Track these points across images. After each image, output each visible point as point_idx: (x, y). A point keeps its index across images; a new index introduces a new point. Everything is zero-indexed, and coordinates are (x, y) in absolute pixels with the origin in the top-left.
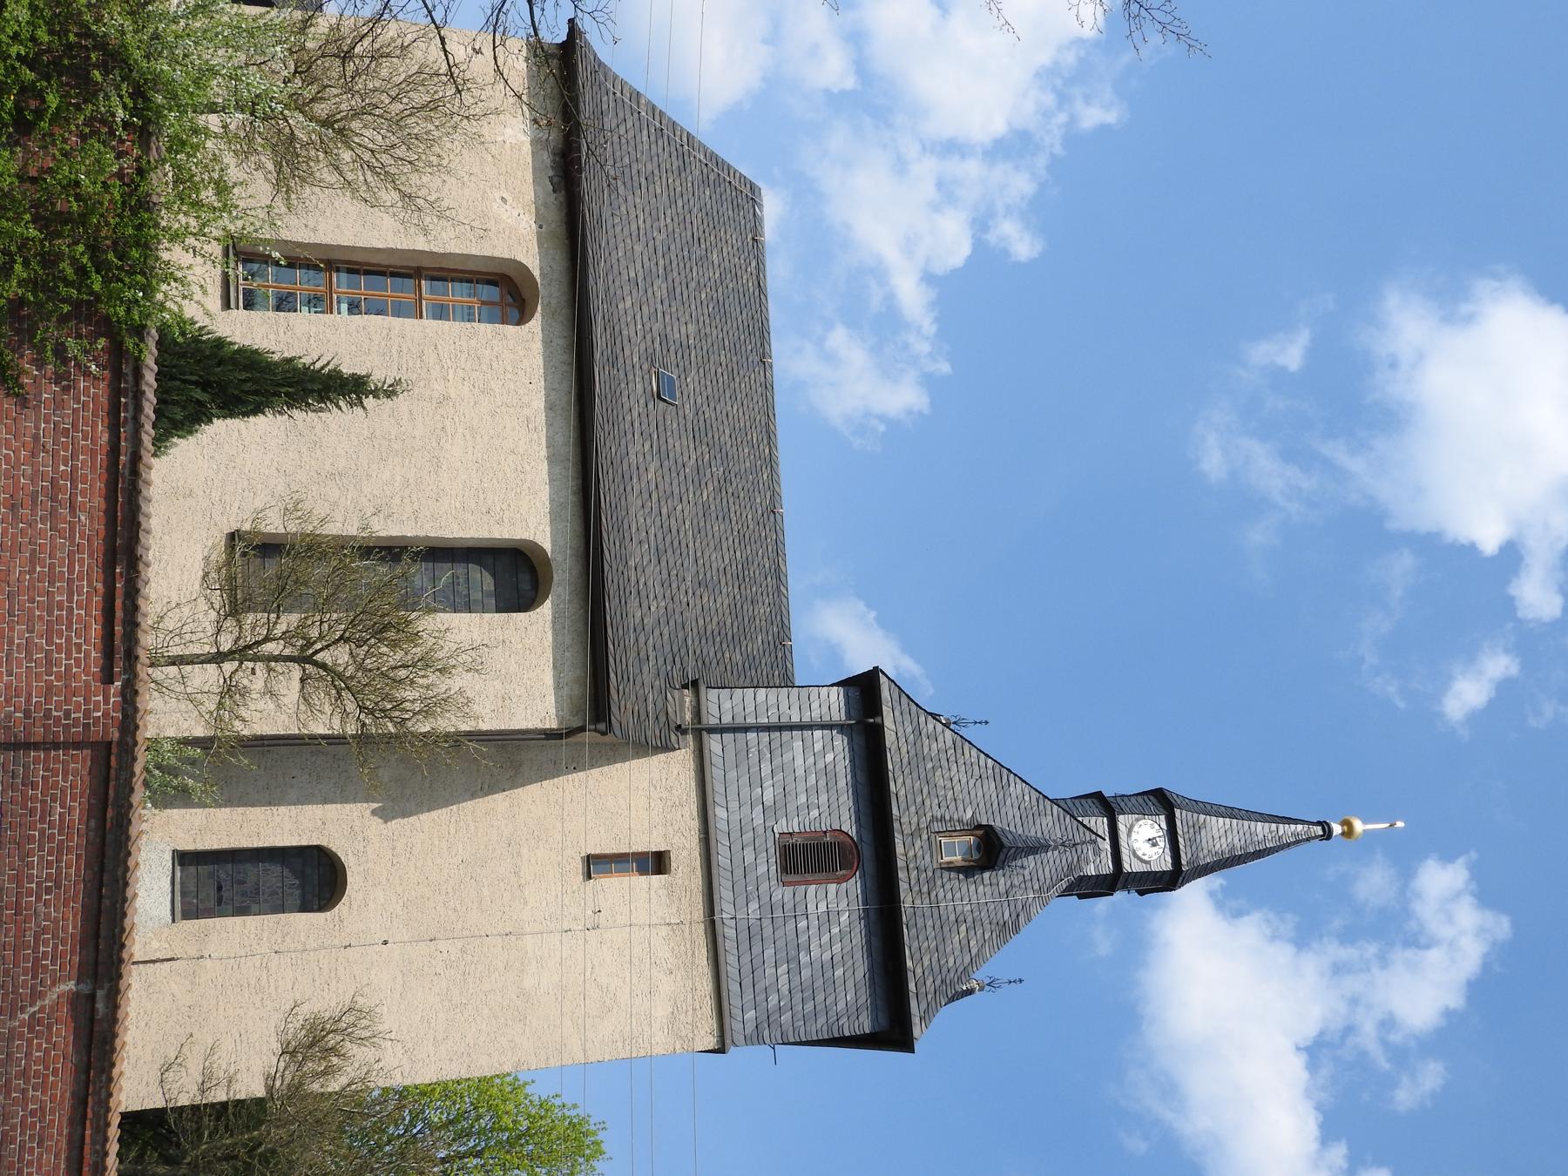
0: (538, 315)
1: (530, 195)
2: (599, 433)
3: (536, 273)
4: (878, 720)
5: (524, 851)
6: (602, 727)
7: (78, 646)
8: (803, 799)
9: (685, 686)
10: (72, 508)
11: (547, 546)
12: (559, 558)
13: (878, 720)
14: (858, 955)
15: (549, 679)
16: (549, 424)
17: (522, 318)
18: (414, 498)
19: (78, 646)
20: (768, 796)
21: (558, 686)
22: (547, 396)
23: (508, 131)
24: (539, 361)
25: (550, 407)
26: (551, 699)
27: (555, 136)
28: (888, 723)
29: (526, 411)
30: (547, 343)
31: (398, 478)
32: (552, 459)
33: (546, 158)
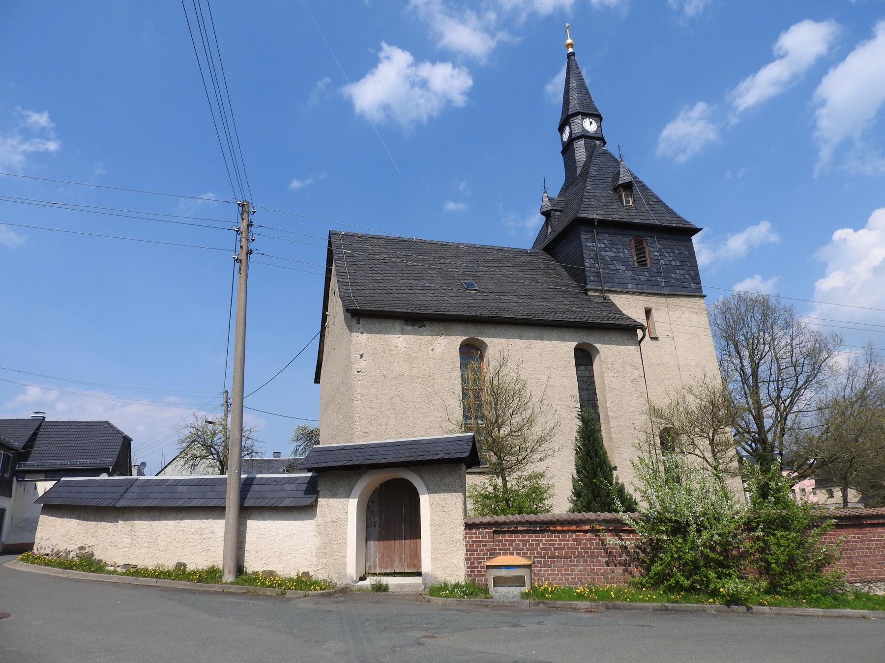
0: (483, 339)
1: (429, 338)
3: (464, 338)
6: (640, 332)
7: (512, 545)
10: (848, 542)
11: (575, 344)
14: (670, 243)
15: (622, 348)
19: (503, 545)
21: (625, 344)
23: (399, 345)
24: (502, 340)
25: (520, 337)
26: (630, 347)
27: (398, 325)
30: (494, 336)
32: (542, 339)
33: (409, 328)
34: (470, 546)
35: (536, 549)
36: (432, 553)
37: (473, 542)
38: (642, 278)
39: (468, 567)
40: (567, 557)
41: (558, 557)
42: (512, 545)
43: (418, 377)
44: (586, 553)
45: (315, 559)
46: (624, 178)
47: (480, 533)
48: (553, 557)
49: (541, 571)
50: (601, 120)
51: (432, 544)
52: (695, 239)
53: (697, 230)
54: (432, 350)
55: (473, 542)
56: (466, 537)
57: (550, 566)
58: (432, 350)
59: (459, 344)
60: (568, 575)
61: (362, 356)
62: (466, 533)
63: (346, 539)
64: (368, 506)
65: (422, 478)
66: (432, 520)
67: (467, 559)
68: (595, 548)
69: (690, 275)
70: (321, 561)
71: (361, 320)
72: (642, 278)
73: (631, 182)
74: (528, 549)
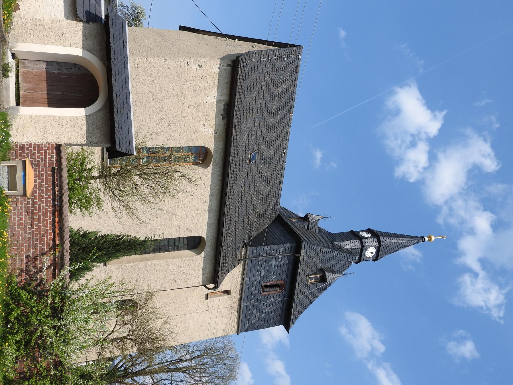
0: (211, 165)
1: (213, 122)
2: (227, 209)
3: (212, 151)
4: (299, 255)
5: (189, 294)
6: (213, 286)
8: (272, 273)
9: (243, 247)
12: (208, 240)
13: (299, 255)
15: (201, 273)
16: (210, 200)
17: (206, 166)
18: (164, 228)
20: (262, 274)
21: (203, 274)
22: (211, 191)
23: (209, 98)
25: (211, 195)
26: (201, 278)
28: (301, 257)
29: (203, 197)
30: (213, 174)
31: (159, 223)
32: (209, 211)
33: (222, 107)
34: (42, 148)
35: (39, 201)
37: (45, 150)
38: (254, 288)
39: (24, 145)
40: (33, 225)
41: (33, 218)
43: (182, 112)
45: (31, 16)
48: (33, 214)
50: (374, 260)
51: (44, 116)
53: (287, 328)
56: (49, 144)
57: (25, 211)
59: (207, 146)
61: (201, 67)
62: (52, 145)
64: (75, 64)
65: (99, 111)
66: (64, 117)
67: (31, 145)
69: (255, 323)
70: (29, 21)
71: (229, 68)
72: (254, 288)
74: (39, 194)
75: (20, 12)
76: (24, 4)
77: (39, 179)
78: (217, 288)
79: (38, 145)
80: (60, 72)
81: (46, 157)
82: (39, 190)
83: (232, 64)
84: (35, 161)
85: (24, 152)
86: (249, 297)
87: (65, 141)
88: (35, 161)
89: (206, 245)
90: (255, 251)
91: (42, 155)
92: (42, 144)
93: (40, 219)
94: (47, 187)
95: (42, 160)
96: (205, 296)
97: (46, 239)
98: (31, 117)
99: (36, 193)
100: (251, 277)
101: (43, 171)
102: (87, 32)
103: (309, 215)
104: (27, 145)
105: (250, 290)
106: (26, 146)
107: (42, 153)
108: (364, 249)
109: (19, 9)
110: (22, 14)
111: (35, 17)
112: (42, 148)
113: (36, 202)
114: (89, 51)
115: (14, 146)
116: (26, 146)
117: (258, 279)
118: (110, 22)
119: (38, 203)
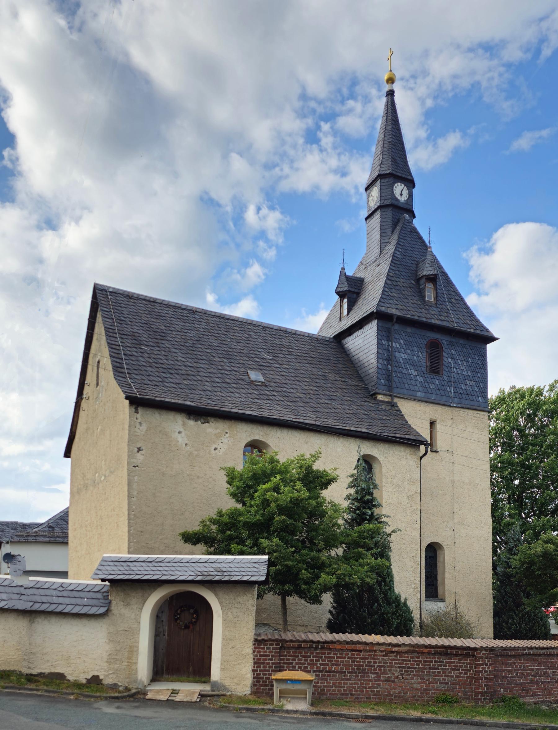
4: (395, 317)
6: (423, 448)
8: (415, 358)
20: (414, 372)
28: (398, 313)
34: (258, 659)
35: (316, 664)
36: (221, 664)
37: (261, 656)
38: (432, 386)
39: (254, 678)
40: (341, 672)
41: (334, 672)
42: (295, 660)
43: (198, 477)
44: (358, 669)
45: (105, 664)
46: (427, 270)
47: (267, 648)
48: (330, 671)
49: (318, 683)
50: (414, 186)
51: (222, 656)
52: (490, 347)
53: (492, 339)
54: (215, 449)
55: (261, 656)
56: (254, 652)
57: (326, 679)
58: (215, 449)
60: (341, 687)
61: (139, 450)
62: (255, 648)
63: (138, 647)
64: (157, 616)
65: (216, 595)
66: (224, 634)
67: (254, 671)
68: (366, 666)
69: (479, 387)
70: (112, 666)
71: (140, 410)
72: (432, 386)
73: (436, 275)
74: (308, 664)
75: (102, 675)
76: (92, 671)
77: (292, 663)
78: (427, 442)
79: (255, 663)
80: (166, 634)
81: (269, 656)
82: (304, 664)
83: (134, 407)
84: (272, 667)
85: (262, 678)
86: (442, 393)
87: (251, 634)
88: (272, 667)
89: (370, 453)
90: (383, 381)
91: (266, 660)
92: (254, 659)
93: (336, 665)
94: (302, 656)
95: (272, 660)
96: (435, 454)
97: (358, 659)
98: (222, 669)
99: (307, 667)
100: (417, 389)
101: (283, 660)
102: (122, 603)
103: (338, 290)
104: (254, 675)
105: (434, 392)
106: (255, 675)
107: (263, 660)
108: (396, 203)
109: (98, 676)
110: (103, 673)
111: (106, 660)
112: (258, 659)
113: (317, 668)
114: (145, 602)
115: (255, 688)
116: (255, 675)
117: (420, 379)
118: (110, 577)
119: (319, 665)
